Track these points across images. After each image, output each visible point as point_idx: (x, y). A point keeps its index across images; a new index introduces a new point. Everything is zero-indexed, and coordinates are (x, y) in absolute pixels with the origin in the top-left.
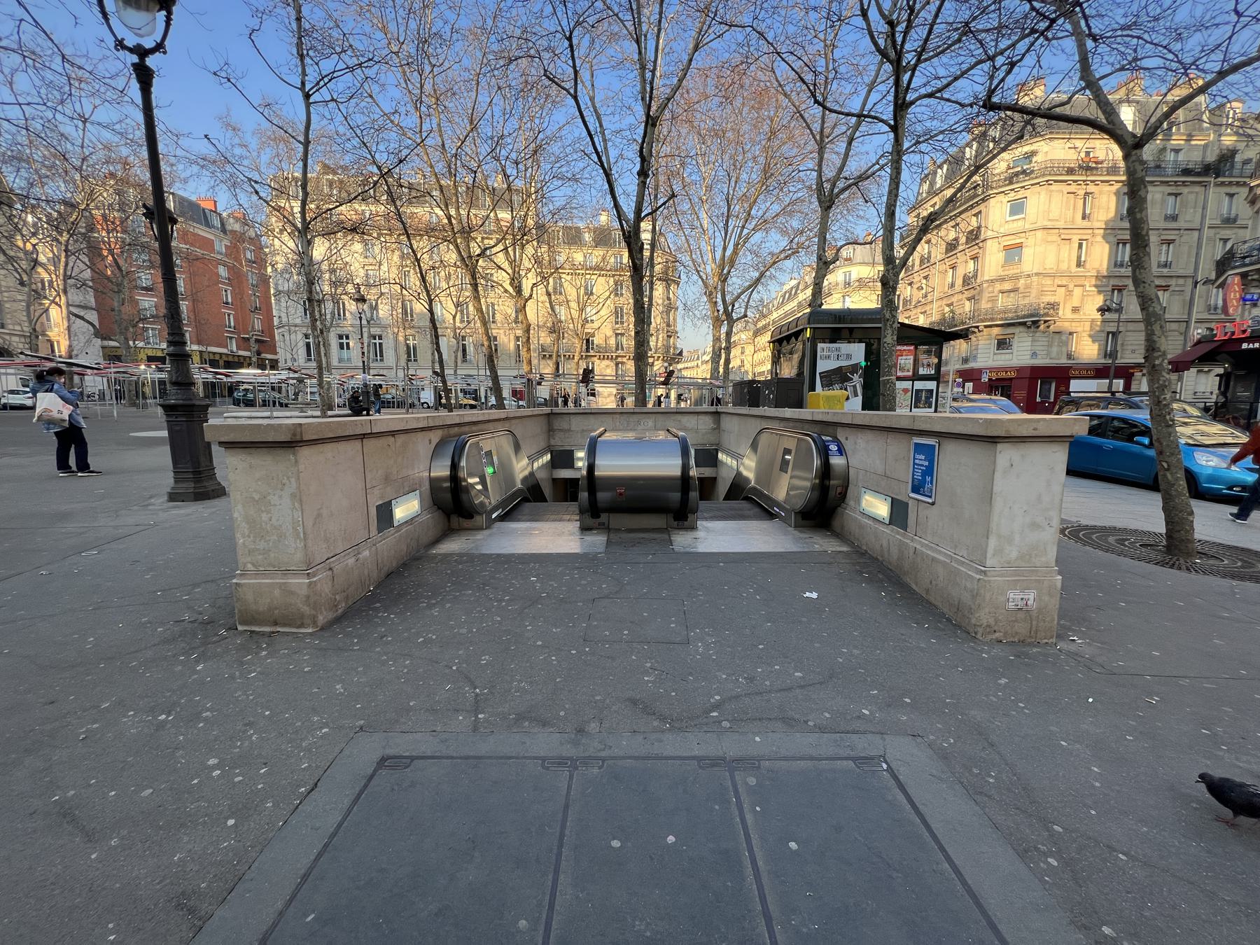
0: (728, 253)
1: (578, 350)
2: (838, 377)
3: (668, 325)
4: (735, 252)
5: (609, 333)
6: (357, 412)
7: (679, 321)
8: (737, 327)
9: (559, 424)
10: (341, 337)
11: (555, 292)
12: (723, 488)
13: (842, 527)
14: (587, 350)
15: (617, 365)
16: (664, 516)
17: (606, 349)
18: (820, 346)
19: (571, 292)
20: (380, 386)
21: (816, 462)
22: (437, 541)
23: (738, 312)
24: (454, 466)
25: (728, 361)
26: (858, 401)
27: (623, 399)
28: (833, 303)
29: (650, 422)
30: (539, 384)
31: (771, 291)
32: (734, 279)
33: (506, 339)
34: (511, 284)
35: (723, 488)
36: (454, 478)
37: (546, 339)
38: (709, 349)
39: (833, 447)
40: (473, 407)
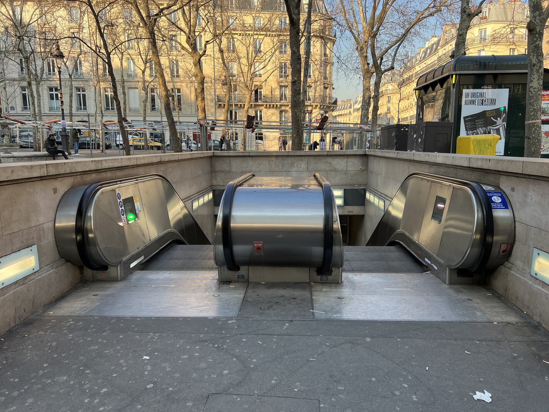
0: (378, 13)
1: (247, 100)
2: (481, 121)
3: (325, 78)
4: (384, 11)
5: (275, 85)
6: (53, 154)
7: (334, 73)
8: (385, 79)
9: (220, 165)
10: (51, 89)
11: (228, 50)
12: (369, 228)
13: (506, 289)
14: (256, 100)
15: (281, 112)
16: (307, 269)
17: (272, 99)
18: (465, 91)
19: (242, 50)
20: (79, 131)
21: (477, 215)
22: (62, 297)
23: (386, 64)
24: (81, 214)
25: (376, 108)
26: (501, 146)
27: (285, 143)
28: (472, 52)
29: (303, 164)
30: (213, 129)
31: (416, 46)
32: (383, 36)
33: (188, 92)
34: (188, 42)
35: (369, 228)
36: (80, 229)
37: (221, 91)
38: (360, 99)
39: (497, 199)
40: (159, 148)
